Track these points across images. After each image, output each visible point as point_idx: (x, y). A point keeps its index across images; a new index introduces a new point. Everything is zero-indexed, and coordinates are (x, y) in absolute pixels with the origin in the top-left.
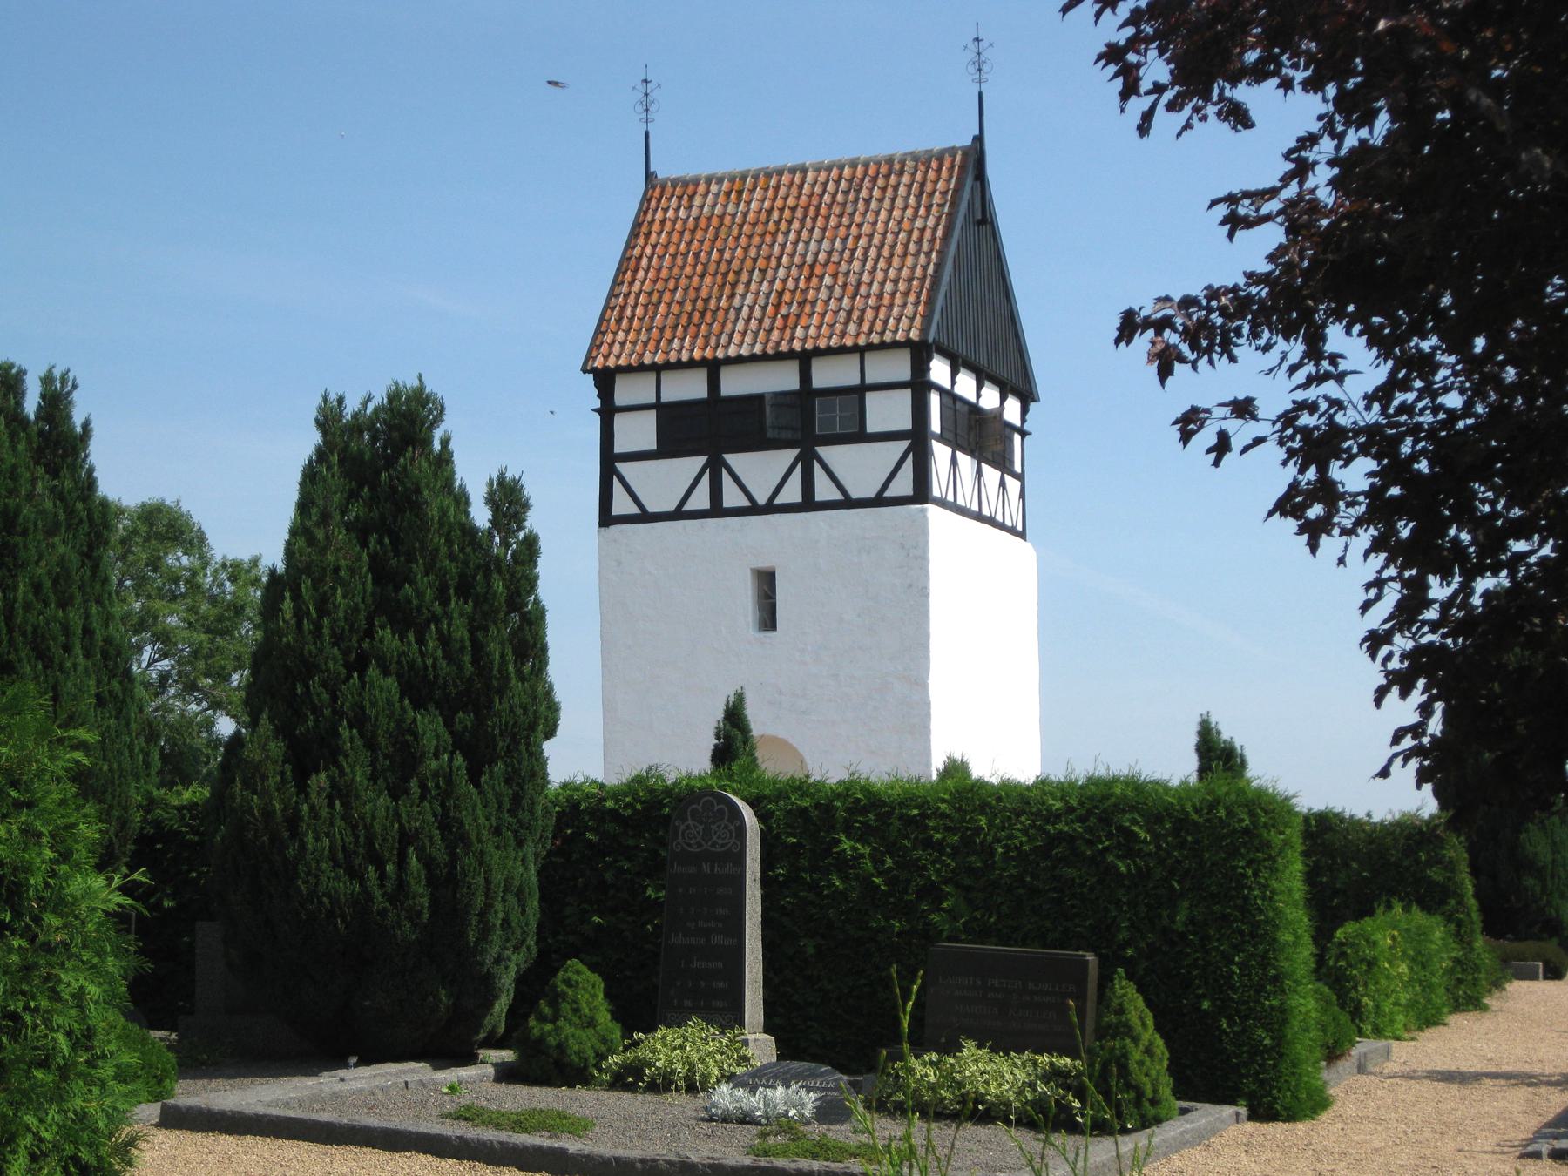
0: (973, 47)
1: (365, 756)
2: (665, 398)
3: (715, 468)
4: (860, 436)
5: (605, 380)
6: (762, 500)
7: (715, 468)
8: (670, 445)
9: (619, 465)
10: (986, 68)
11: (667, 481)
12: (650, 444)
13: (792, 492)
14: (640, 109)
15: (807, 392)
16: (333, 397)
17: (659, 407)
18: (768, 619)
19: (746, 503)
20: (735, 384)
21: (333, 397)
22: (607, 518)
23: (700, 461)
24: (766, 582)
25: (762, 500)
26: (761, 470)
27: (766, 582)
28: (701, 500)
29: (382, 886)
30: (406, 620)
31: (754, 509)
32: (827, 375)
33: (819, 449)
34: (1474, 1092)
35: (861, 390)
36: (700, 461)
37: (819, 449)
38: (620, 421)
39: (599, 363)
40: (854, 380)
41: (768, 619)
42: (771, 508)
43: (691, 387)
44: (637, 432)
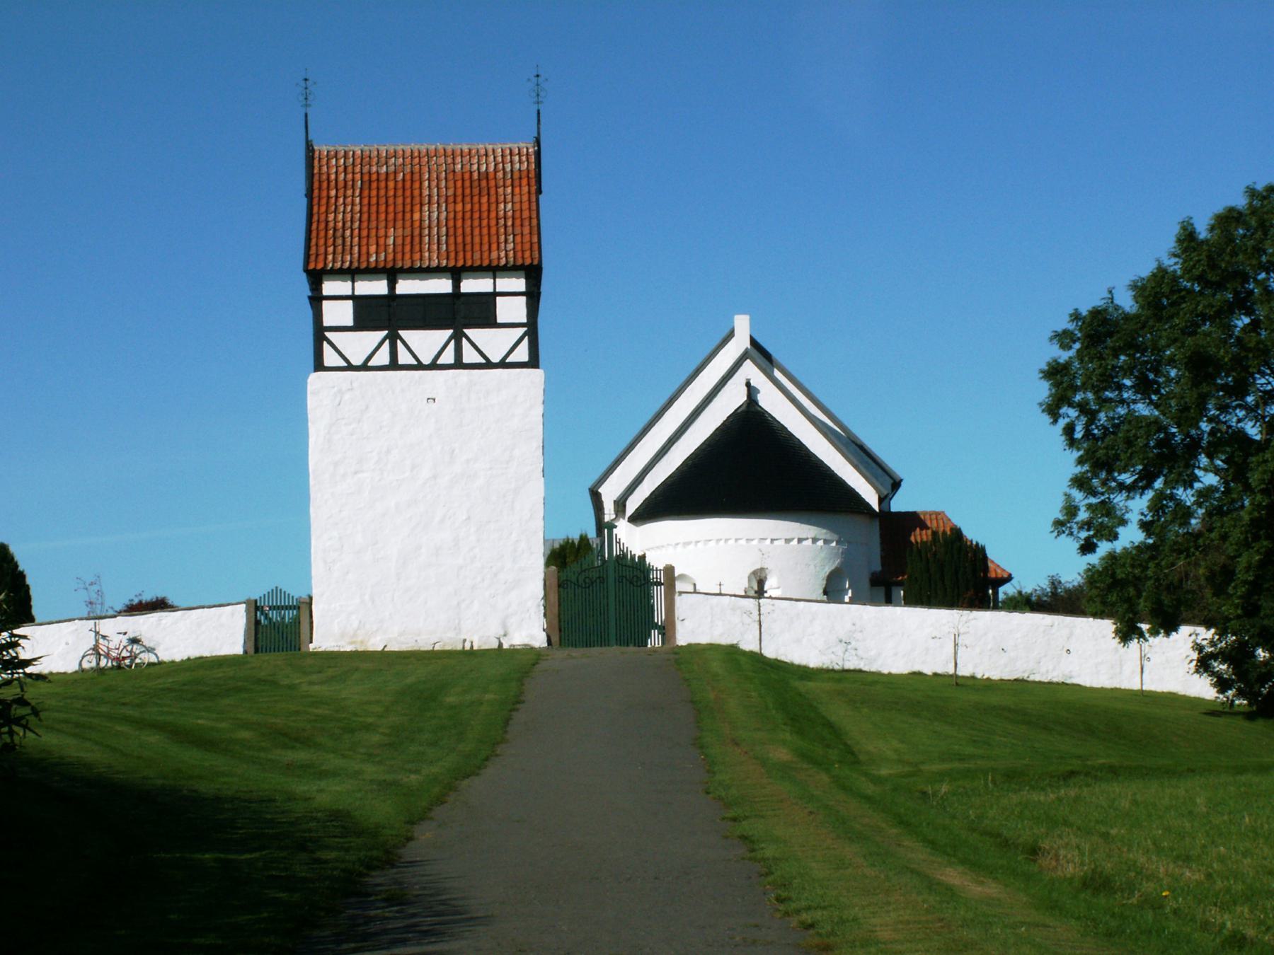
0: (303, 84)
2: (357, 293)
5: (316, 278)
6: (426, 361)
7: (393, 338)
9: (328, 334)
10: (310, 98)
12: (350, 323)
13: (448, 357)
14: (302, 98)
15: (456, 294)
17: (352, 297)
19: (344, 364)
20: (406, 287)
23: (450, 332)
25: (426, 361)
26: (425, 342)
28: (383, 357)
29: (928, 564)
31: (420, 366)
32: (471, 285)
33: (400, 332)
36: (450, 332)
37: (400, 332)
39: (312, 266)
40: (491, 290)
42: (434, 366)
43: (378, 287)
44: (338, 313)
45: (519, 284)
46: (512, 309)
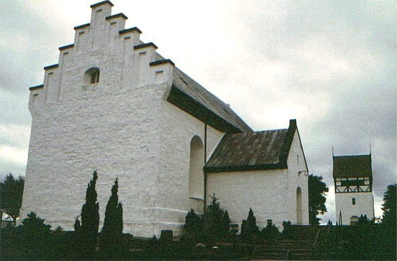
1: (73, 163)
3: (348, 187)
4: (364, 185)
6: (353, 191)
7: (348, 187)
8: (342, 185)
11: (342, 189)
16: (364, 215)
18: (354, 203)
20: (349, 179)
21: (364, 215)
22: (336, 192)
24: (354, 200)
26: (353, 188)
27: (354, 200)
28: (346, 191)
30: (62, 118)
31: (352, 192)
32: (359, 179)
34: (301, 149)
35: (364, 180)
38: (337, 183)
41: (354, 203)
42: (354, 192)
44: (340, 184)
45: (368, 178)
46: (367, 183)
